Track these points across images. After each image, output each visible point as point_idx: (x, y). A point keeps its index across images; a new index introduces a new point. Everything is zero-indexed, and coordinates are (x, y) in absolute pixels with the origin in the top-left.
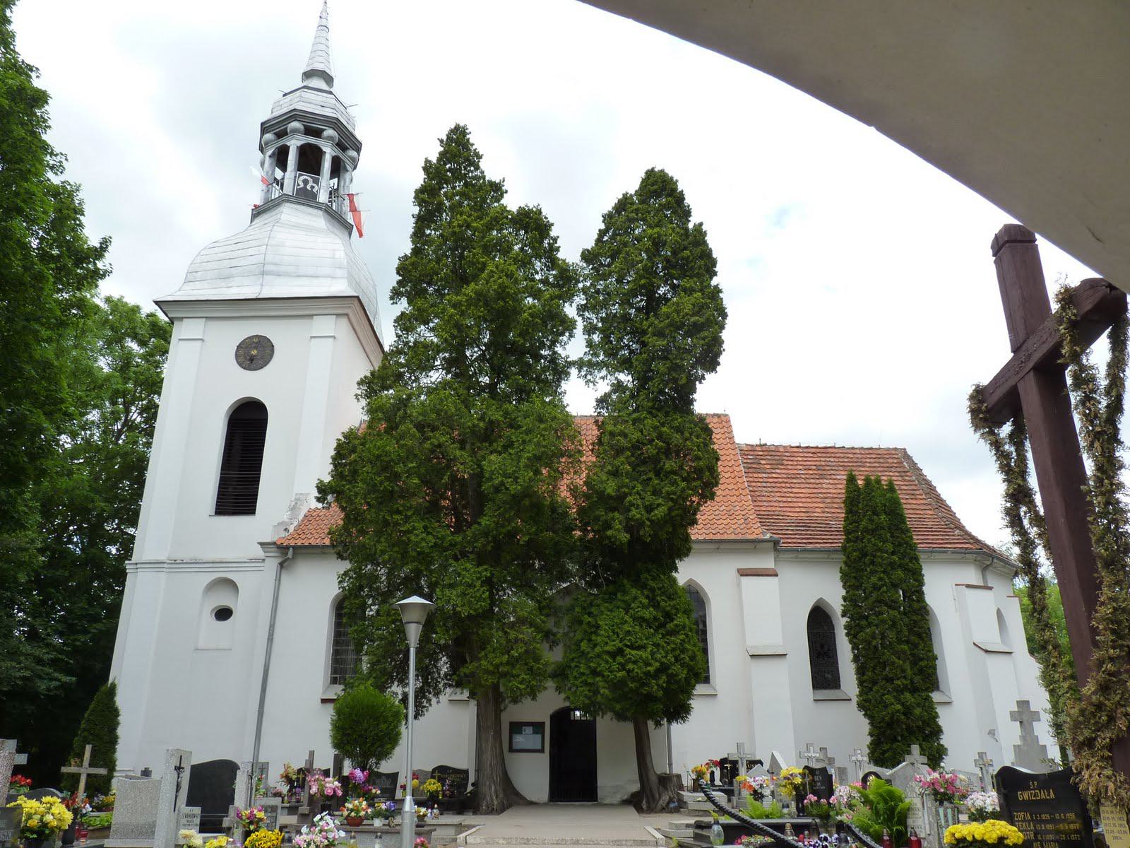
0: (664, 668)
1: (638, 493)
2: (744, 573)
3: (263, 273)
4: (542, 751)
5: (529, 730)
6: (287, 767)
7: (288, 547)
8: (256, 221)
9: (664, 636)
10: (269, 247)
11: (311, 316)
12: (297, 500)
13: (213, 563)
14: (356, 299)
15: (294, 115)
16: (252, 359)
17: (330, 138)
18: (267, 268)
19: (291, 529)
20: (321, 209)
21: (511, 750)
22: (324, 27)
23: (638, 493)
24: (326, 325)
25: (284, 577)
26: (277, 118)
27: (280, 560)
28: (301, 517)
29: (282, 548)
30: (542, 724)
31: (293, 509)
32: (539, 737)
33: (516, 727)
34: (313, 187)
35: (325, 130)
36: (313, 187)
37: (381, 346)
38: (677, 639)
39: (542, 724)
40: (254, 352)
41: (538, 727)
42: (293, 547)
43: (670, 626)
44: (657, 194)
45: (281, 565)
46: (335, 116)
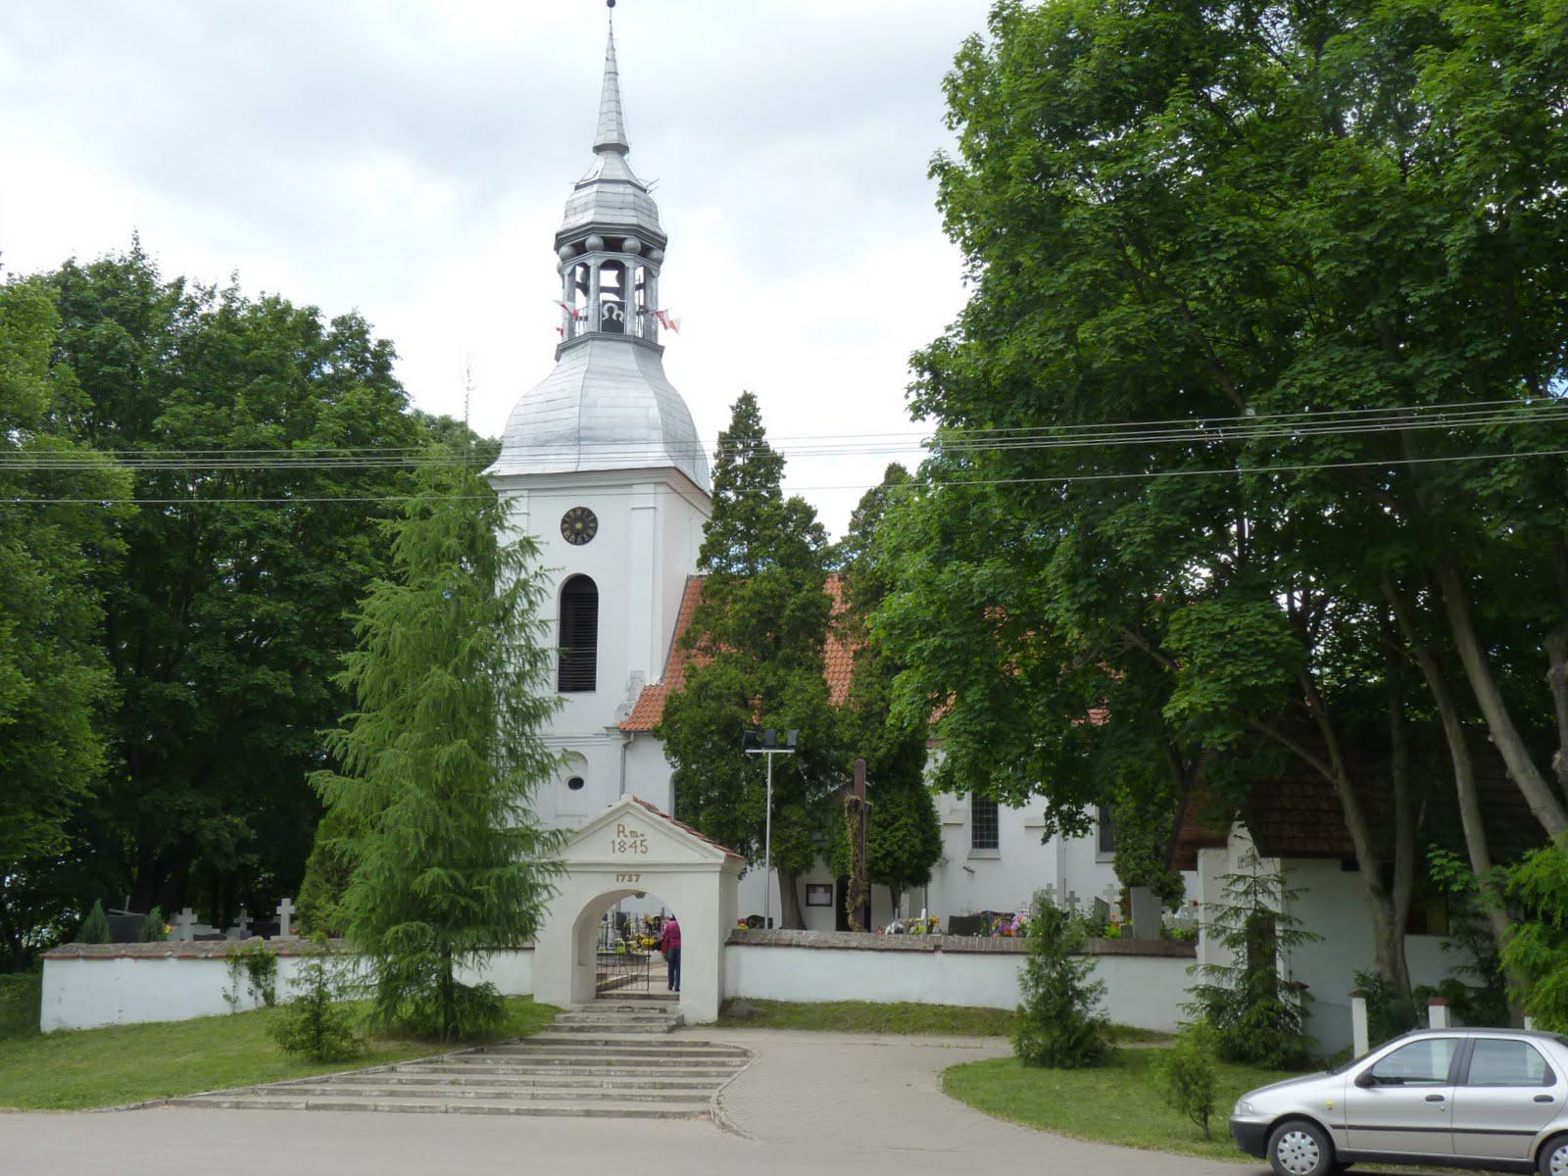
0: (889, 854)
1: (867, 739)
3: (580, 439)
4: (830, 905)
5: (822, 890)
6: (646, 917)
7: (629, 732)
8: (564, 357)
9: (891, 832)
10: (583, 409)
11: (630, 485)
12: (633, 678)
13: (663, 1115)
14: (674, 472)
15: (592, 228)
16: (577, 533)
17: (632, 250)
18: (584, 433)
19: (631, 712)
20: (630, 342)
21: (808, 904)
22: (613, 74)
23: (867, 739)
24: (645, 496)
25: (627, 753)
26: (572, 230)
27: (624, 742)
28: (637, 698)
29: (626, 733)
30: (831, 886)
31: (630, 689)
32: (828, 895)
33: (811, 888)
34: (618, 316)
35: (625, 239)
36: (618, 316)
37: (706, 494)
38: (900, 834)
39: (831, 886)
40: (579, 526)
41: (828, 888)
42: (635, 732)
43: (896, 825)
44: (897, 482)
45: (625, 746)
46: (634, 221)
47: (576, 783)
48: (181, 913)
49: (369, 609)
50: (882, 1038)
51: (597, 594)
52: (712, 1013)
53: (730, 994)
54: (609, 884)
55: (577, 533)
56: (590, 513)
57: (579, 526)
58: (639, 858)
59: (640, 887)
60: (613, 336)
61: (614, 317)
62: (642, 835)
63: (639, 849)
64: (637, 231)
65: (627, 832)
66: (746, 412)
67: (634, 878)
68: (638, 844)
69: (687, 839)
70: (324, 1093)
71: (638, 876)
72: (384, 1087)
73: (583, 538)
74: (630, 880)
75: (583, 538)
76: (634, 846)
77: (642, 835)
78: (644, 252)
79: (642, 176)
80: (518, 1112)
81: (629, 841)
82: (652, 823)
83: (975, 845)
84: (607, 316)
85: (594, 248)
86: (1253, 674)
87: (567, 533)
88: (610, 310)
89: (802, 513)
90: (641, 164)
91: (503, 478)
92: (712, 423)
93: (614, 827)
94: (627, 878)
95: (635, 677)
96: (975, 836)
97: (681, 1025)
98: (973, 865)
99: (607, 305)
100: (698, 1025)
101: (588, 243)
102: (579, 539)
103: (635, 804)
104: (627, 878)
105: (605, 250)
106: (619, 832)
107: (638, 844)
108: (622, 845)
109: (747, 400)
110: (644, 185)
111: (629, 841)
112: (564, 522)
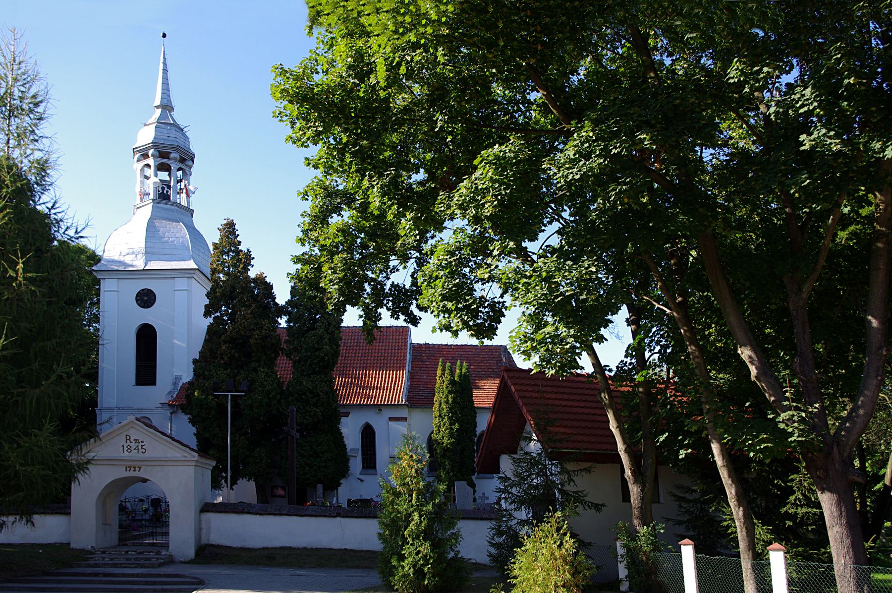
2: (391, 419)
14: (197, 271)
31: (175, 384)
34: (167, 192)
36: (167, 192)
50: (749, 571)
52: (191, 553)
53: (204, 541)
54: (121, 473)
55: (142, 300)
57: (146, 298)
59: (142, 474)
60: (164, 201)
62: (142, 442)
63: (141, 450)
64: (177, 148)
65: (132, 440)
66: (230, 229)
67: (137, 469)
68: (140, 447)
69: (173, 444)
71: (140, 468)
74: (135, 470)
76: (137, 448)
77: (142, 442)
78: (182, 160)
79: (181, 122)
81: (134, 445)
82: (148, 433)
83: (363, 467)
85: (175, 159)
86: (609, 116)
90: (179, 116)
91: (96, 271)
92: (212, 236)
94: (132, 469)
95: (178, 378)
96: (363, 463)
97: (171, 561)
98: (362, 477)
100: (182, 562)
101: (172, 156)
103: (137, 422)
106: (127, 440)
107: (140, 447)
110: (182, 127)
111: (134, 445)
112: (137, 296)
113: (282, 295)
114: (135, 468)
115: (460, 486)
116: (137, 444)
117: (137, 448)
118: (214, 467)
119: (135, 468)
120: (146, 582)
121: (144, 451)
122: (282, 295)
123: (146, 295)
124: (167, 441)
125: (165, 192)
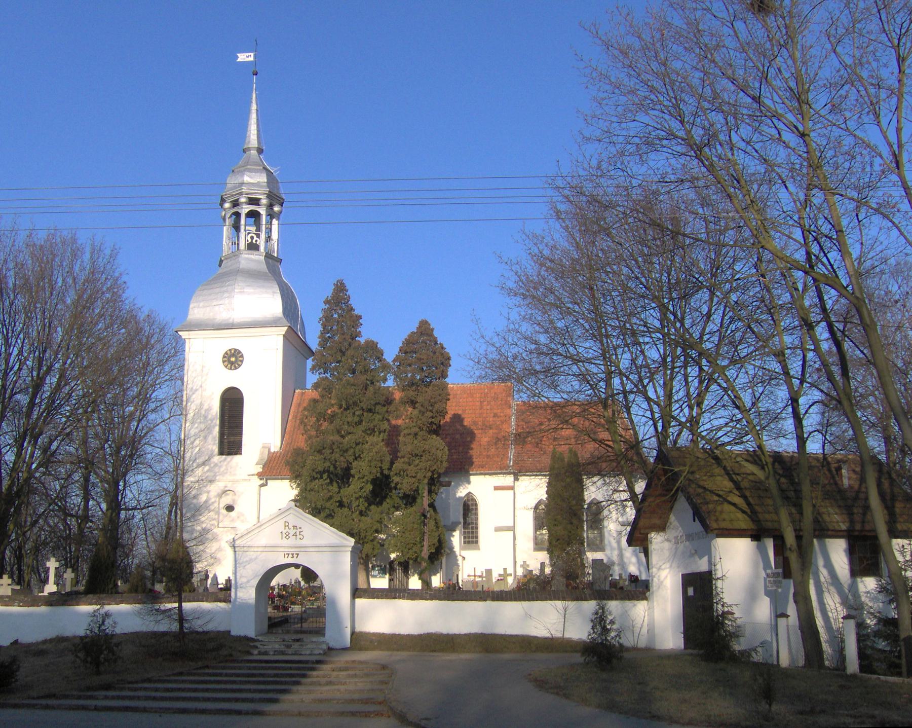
34: (256, 241)
36: (256, 241)
40: (233, 359)
47: (230, 508)
48: (472, 449)
49: (811, 28)
51: (243, 399)
56: (240, 352)
57: (233, 359)
58: (300, 542)
61: (254, 241)
63: (298, 537)
65: (290, 526)
67: (295, 556)
70: (106, 697)
71: (298, 554)
72: (350, 672)
73: (235, 366)
74: (293, 557)
75: (235, 366)
76: (295, 535)
80: (96, 709)
81: (292, 532)
84: (250, 241)
87: (226, 363)
88: (252, 238)
89: (372, 348)
93: (282, 523)
99: (250, 235)
102: (233, 368)
104: (291, 556)
105: (249, 204)
107: (298, 534)
108: (287, 535)
109: (340, 288)
110: (726, 476)
111: (292, 532)
113: (390, 353)
114: (293, 554)
115: (212, 507)
116: (295, 531)
117: (295, 535)
118: (353, 548)
119: (293, 554)
120: (240, 681)
121: (302, 537)
122: (390, 353)
123: (233, 355)
124: (325, 527)
125: (254, 241)
